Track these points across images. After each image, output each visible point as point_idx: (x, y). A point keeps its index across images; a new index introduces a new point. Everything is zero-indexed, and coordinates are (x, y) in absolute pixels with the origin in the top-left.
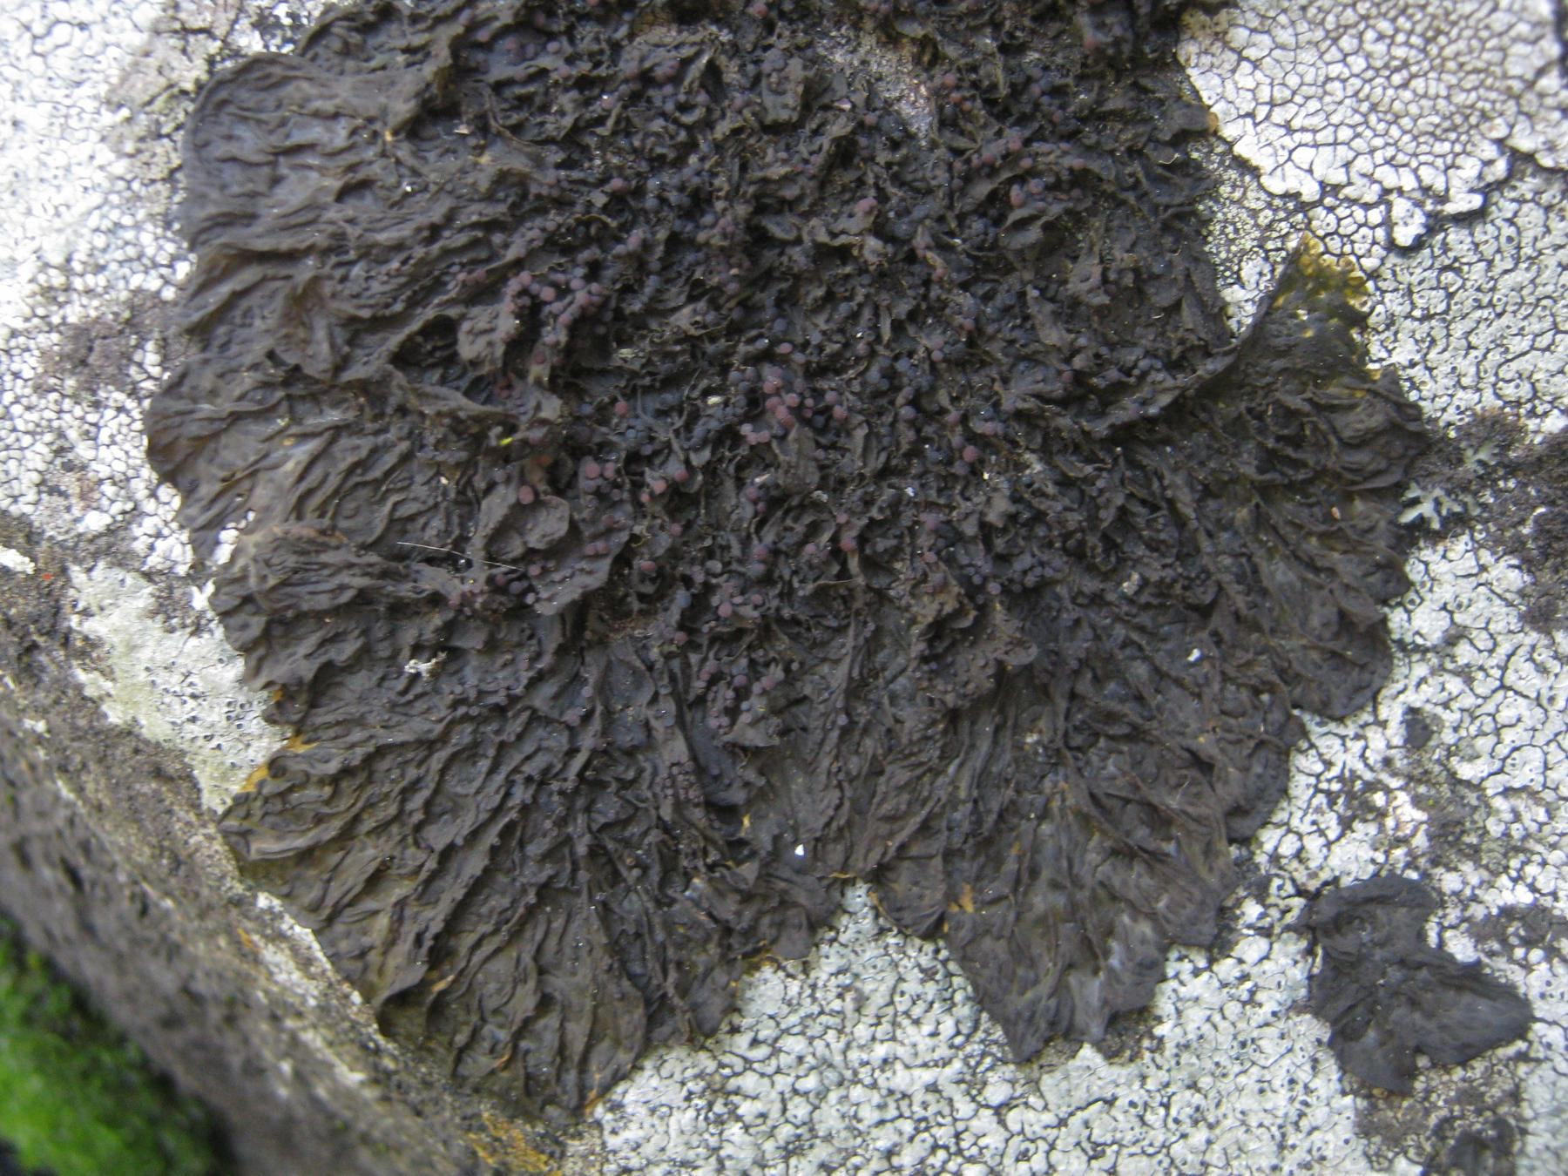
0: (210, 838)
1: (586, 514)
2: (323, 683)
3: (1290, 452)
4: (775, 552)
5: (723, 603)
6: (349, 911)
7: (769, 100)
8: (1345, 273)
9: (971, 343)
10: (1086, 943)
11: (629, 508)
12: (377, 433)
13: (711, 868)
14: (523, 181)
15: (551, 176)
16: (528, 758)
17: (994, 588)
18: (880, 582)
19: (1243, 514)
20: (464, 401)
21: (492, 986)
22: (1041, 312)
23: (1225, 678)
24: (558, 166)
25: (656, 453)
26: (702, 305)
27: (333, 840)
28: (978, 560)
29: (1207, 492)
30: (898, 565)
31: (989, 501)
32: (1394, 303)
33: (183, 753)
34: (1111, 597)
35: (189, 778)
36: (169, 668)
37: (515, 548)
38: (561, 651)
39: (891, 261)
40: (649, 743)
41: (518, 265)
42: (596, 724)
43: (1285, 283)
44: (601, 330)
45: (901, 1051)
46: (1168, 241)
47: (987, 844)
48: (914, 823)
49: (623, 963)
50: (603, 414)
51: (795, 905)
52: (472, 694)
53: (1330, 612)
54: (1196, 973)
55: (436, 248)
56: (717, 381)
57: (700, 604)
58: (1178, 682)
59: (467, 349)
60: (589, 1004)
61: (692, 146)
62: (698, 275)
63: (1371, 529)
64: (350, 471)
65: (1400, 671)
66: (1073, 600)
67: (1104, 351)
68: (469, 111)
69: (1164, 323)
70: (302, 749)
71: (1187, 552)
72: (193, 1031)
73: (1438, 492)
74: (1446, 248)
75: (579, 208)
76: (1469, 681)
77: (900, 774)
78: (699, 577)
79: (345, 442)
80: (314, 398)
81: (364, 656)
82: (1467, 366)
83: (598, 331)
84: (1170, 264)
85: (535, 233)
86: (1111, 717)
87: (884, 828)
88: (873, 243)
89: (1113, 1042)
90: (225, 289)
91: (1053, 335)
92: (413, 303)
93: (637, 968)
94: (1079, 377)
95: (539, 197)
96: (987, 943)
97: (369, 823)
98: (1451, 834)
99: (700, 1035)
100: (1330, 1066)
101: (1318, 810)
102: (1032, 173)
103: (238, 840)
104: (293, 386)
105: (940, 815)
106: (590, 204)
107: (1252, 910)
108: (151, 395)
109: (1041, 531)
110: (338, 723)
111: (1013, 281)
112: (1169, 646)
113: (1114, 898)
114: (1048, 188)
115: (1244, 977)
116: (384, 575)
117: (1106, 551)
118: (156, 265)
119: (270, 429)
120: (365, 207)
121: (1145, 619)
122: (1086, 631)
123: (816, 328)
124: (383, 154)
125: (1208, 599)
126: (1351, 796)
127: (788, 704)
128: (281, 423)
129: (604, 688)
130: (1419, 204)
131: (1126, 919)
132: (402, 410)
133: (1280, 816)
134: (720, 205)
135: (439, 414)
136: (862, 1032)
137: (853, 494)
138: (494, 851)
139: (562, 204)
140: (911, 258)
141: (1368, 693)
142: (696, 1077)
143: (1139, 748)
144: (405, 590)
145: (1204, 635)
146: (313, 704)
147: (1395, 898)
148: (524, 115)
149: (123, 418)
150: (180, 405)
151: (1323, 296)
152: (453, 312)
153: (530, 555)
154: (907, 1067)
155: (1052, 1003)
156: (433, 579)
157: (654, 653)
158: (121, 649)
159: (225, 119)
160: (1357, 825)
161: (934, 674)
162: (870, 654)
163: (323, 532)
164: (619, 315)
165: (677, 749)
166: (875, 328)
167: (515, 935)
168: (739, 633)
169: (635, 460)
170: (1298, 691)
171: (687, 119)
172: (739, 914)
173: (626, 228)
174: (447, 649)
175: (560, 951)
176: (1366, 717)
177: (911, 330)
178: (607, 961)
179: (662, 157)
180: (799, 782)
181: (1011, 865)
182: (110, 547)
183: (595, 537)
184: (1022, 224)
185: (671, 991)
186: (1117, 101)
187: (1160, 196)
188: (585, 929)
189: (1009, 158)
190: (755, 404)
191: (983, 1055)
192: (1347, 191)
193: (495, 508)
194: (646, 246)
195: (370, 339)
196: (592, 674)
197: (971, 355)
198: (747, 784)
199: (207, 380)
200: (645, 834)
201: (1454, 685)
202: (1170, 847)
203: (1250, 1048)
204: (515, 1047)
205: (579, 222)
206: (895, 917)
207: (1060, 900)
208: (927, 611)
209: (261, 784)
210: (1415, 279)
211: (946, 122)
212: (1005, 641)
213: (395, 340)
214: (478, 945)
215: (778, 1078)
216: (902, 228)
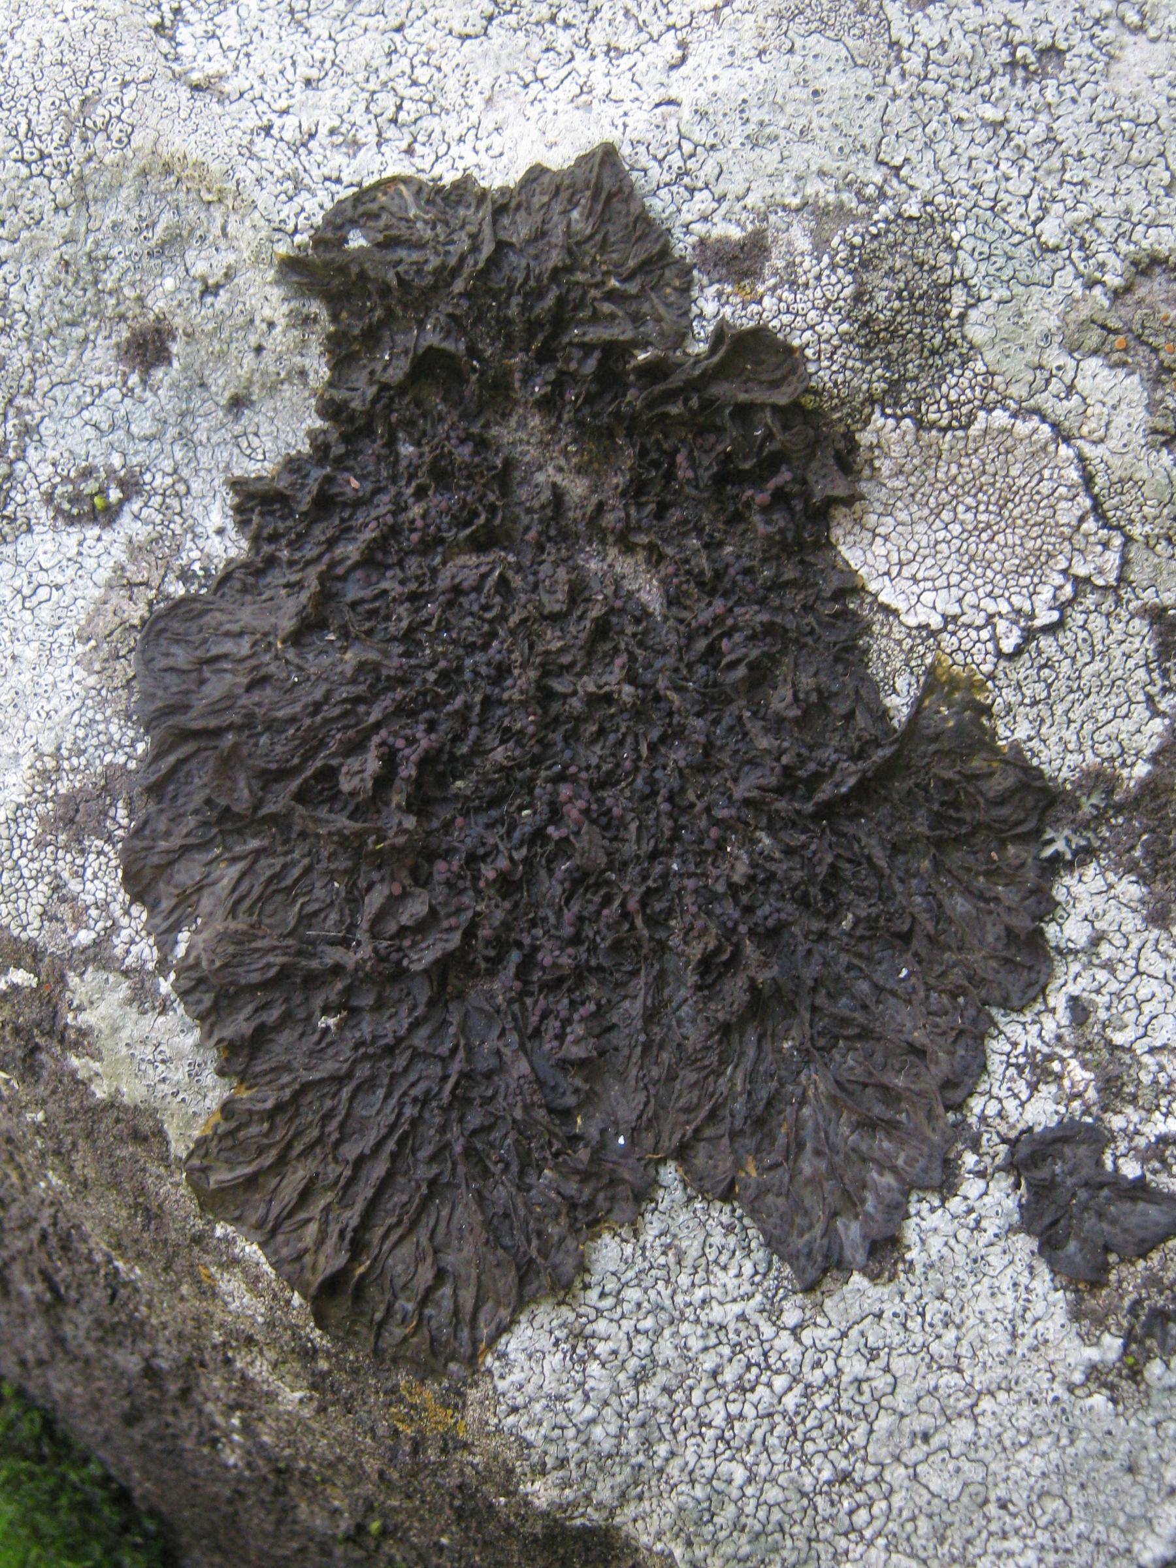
0: (177, 1185)
1: (441, 899)
2: (259, 1039)
3: (951, 812)
4: (580, 919)
6: (287, 1223)
7: (545, 598)
8: (970, 677)
9: (706, 754)
10: (845, 1193)
11: (471, 893)
12: (286, 853)
13: (556, 1155)
14: (376, 667)
15: (396, 662)
16: (413, 1085)
17: (743, 929)
18: (661, 934)
19: (926, 864)
20: (347, 822)
21: (400, 1268)
22: (754, 727)
23: (929, 988)
24: (401, 656)
25: (487, 855)
26: (511, 744)
27: (270, 1167)
28: (731, 910)
29: (895, 850)
30: (673, 923)
31: (732, 867)
32: (1009, 695)
33: (156, 1110)
34: (833, 933)
35: (160, 1133)
36: (144, 1042)
37: (392, 927)
38: (431, 1003)
39: (643, 701)
40: (501, 1068)
41: (377, 726)
42: (461, 1054)
44: (441, 768)
45: (715, 1292)
46: (840, 668)
47: (761, 1122)
48: (703, 1113)
49: (497, 1238)
50: (447, 826)
51: (622, 1181)
52: (369, 1037)
53: (1000, 930)
54: (933, 1210)
55: (318, 718)
56: (527, 799)
57: (528, 963)
58: (893, 993)
59: (346, 785)
60: (474, 1273)
61: (493, 635)
62: (506, 723)
63: (1023, 865)
64: (269, 881)
65: (1060, 969)
66: (806, 937)
67: (803, 751)
68: (335, 623)
69: (845, 728)
70: (245, 1095)
71: (885, 896)
73: (1067, 832)
74: (1040, 653)
75: (418, 683)
78: (527, 940)
79: (263, 862)
80: (239, 832)
81: (287, 1019)
82: (1069, 735)
83: (437, 768)
84: (844, 685)
85: (388, 702)
86: (844, 1022)
87: (683, 1118)
88: (628, 689)
89: (875, 1267)
90: (172, 759)
91: (764, 743)
92: (305, 759)
93: (507, 1241)
94: (787, 770)
95: (388, 678)
96: (770, 1199)
97: (298, 1148)
100: (1043, 1269)
101: (1012, 1079)
102: (735, 628)
103: (197, 1177)
104: (226, 823)
105: (723, 1105)
106: (425, 681)
107: (970, 1159)
108: (122, 839)
109: (775, 887)
110: (272, 1070)
111: (733, 708)
112: (884, 966)
113: (864, 1160)
114: (748, 638)
115: (971, 1210)
116: (299, 953)
117: (826, 901)
118: (121, 747)
119: (210, 856)
120: (268, 694)
121: (863, 948)
122: (816, 959)
123: (594, 755)
124: (277, 658)
125: (906, 927)
126: (1034, 1066)
128: (217, 851)
129: (464, 1029)
130: (1015, 623)
131: (875, 1175)
132: (303, 835)
133: (982, 1087)
134: (516, 672)
135: (330, 834)
136: (684, 1280)
137: (633, 871)
138: (394, 1156)
139: (404, 682)
140: (658, 698)
141: (1037, 988)
142: (561, 1326)
143: (869, 1045)
145: (908, 956)
146: (252, 1057)
148: (373, 623)
149: (102, 859)
150: (145, 843)
151: (957, 695)
152: (334, 762)
153: (403, 930)
154: (721, 1303)
155: (825, 1241)
156: (333, 955)
157: (500, 999)
158: (107, 1032)
159: (163, 642)
160: (1041, 1087)
161: (707, 999)
162: (659, 989)
163: (252, 926)
164: (453, 758)
166: (636, 749)
167: (414, 1224)
168: (560, 981)
169: (473, 859)
170: (983, 993)
171: (488, 615)
172: (580, 1191)
173: (452, 696)
175: (448, 1234)
176: (1038, 1006)
177: (663, 750)
178: (484, 1235)
179: (473, 644)
181: (781, 1140)
183: (449, 916)
184: (733, 665)
185: (534, 1254)
186: (790, 573)
187: (829, 637)
188: (464, 1213)
189: (718, 620)
190: (555, 814)
191: (777, 1288)
192: (963, 619)
193: (374, 901)
194: (468, 707)
195: (276, 787)
196: (455, 1018)
197: (705, 766)
198: (577, 1091)
199: (162, 826)
200: (505, 1136)
202: (903, 1117)
203: (981, 1263)
204: (421, 1314)
205: (418, 693)
208: (696, 951)
209: (216, 1126)
210: (1021, 676)
211: (672, 601)
213: (294, 785)
214: (386, 1236)
215: (624, 1322)
216: (648, 677)
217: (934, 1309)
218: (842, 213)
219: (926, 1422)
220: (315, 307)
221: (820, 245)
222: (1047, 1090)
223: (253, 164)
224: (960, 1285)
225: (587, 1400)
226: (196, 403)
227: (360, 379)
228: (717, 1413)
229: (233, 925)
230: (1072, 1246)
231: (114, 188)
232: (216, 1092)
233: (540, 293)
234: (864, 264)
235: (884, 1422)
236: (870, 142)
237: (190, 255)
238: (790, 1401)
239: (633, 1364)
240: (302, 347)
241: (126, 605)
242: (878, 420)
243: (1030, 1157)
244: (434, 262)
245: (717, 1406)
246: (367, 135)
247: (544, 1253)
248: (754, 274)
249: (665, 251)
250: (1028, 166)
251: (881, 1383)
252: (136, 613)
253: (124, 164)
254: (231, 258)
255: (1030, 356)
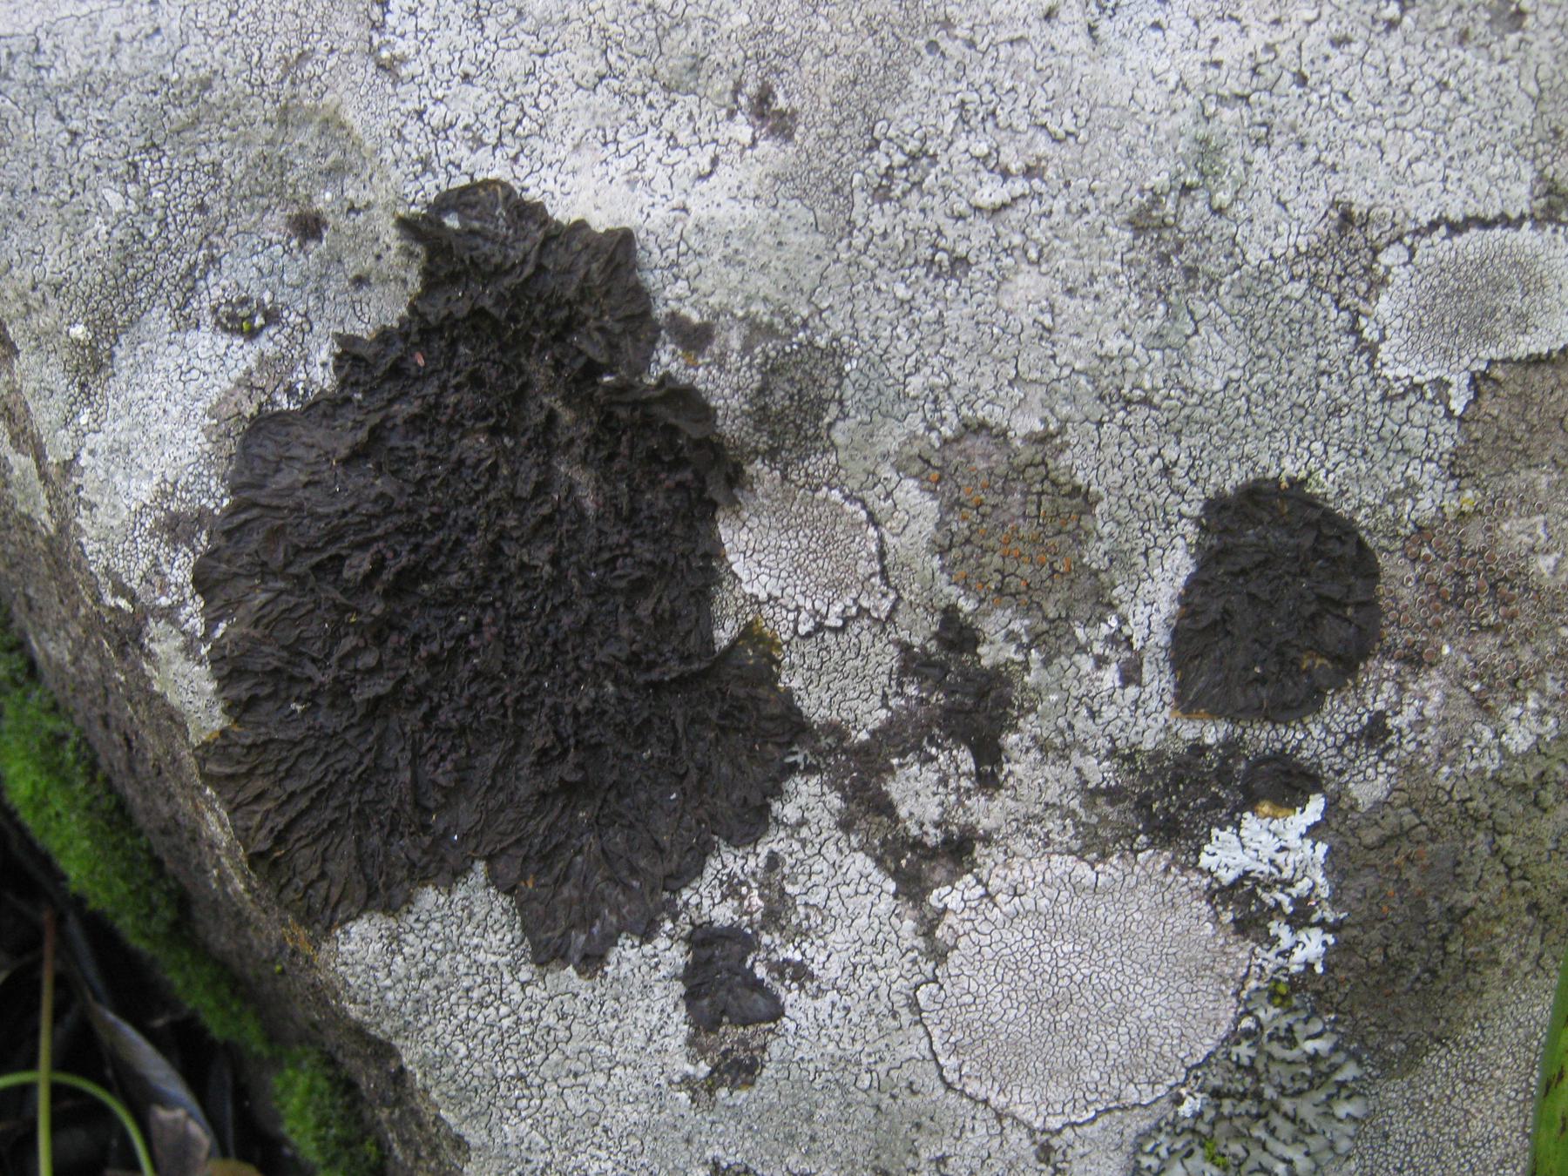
2: (251, 703)
5: (444, 715)
22: (624, 618)
32: (795, 658)
38: (365, 716)
43: (742, 635)
47: (546, 858)
50: (407, 614)
71: (675, 749)
72: (176, 840)
76: (804, 846)
77: (511, 814)
81: (272, 696)
82: (826, 697)
86: (621, 816)
88: (548, 568)
90: (243, 517)
96: (535, 905)
98: (774, 916)
99: (390, 909)
103: (202, 761)
104: (264, 571)
107: (668, 925)
120: (315, 494)
127: (463, 771)
129: (380, 738)
136: (469, 929)
138: (313, 800)
139: (410, 511)
144: (297, 672)
147: (738, 940)
156: (310, 670)
157: (408, 729)
165: (406, 776)
167: (315, 841)
169: (416, 639)
174: (312, 700)
180: (463, 805)
181: (556, 871)
182: (169, 614)
184: (620, 577)
188: (348, 847)
190: (478, 626)
193: (348, 644)
196: (376, 731)
197: (585, 629)
201: (796, 846)
202: (635, 884)
206: (493, 879)
207: (575, 894)
212: (567, 771)
213: (316, 559)
217: (610, 1005)
218: (770, 331)
219: (579, 1066)
220: (418, 248)
221: (747, 348)
222: (732, 903)
223: (397, 147)
224: (630, 997)
225: (389, 974)
226: (332, 271)
227: (440, 299)
228: (462, 1011)
229: (253, 632)
230: (705, 1002)
231: (306, 121)
232: (219, 721)
233: (559, 307)
234: (773, 371)
235: (555, 1057)
236: (807, 286)
237: (348, 181)
238: (506, 1023)
239: (422, 966)
240: (407, 268)
241: (246, 403)
242: (758, 464)
243: (704, 939)
244: (497, 259)
245: (463, 1008)
246: (490, 137)
247: (387, 887)
248: (700, 350)
249: (647, 313)
250: (917, 336)
251: (562, 1034)
252: (250, 409)
253: (315, 110)
254: (372, 197)
255: (869, 465)
